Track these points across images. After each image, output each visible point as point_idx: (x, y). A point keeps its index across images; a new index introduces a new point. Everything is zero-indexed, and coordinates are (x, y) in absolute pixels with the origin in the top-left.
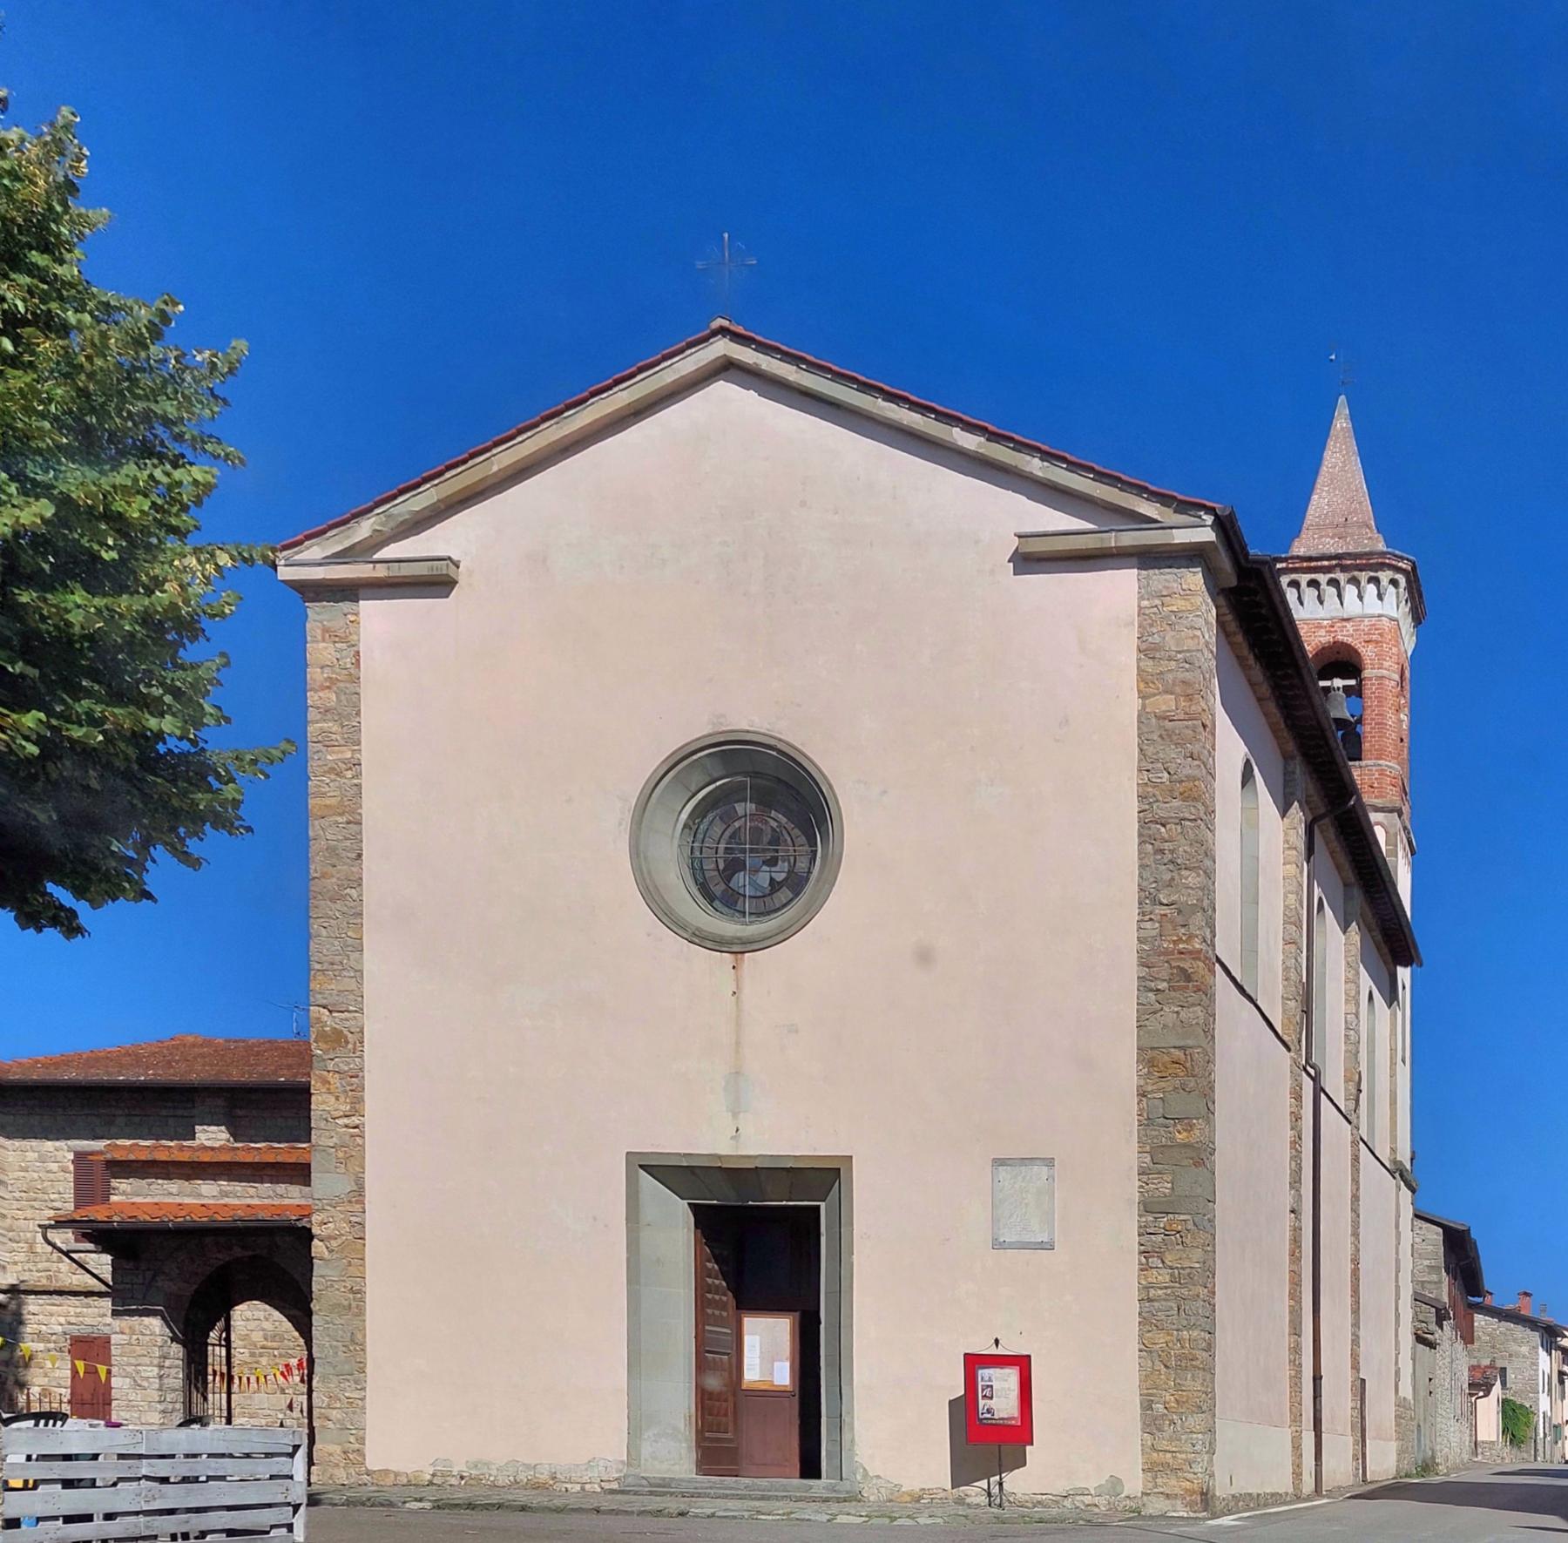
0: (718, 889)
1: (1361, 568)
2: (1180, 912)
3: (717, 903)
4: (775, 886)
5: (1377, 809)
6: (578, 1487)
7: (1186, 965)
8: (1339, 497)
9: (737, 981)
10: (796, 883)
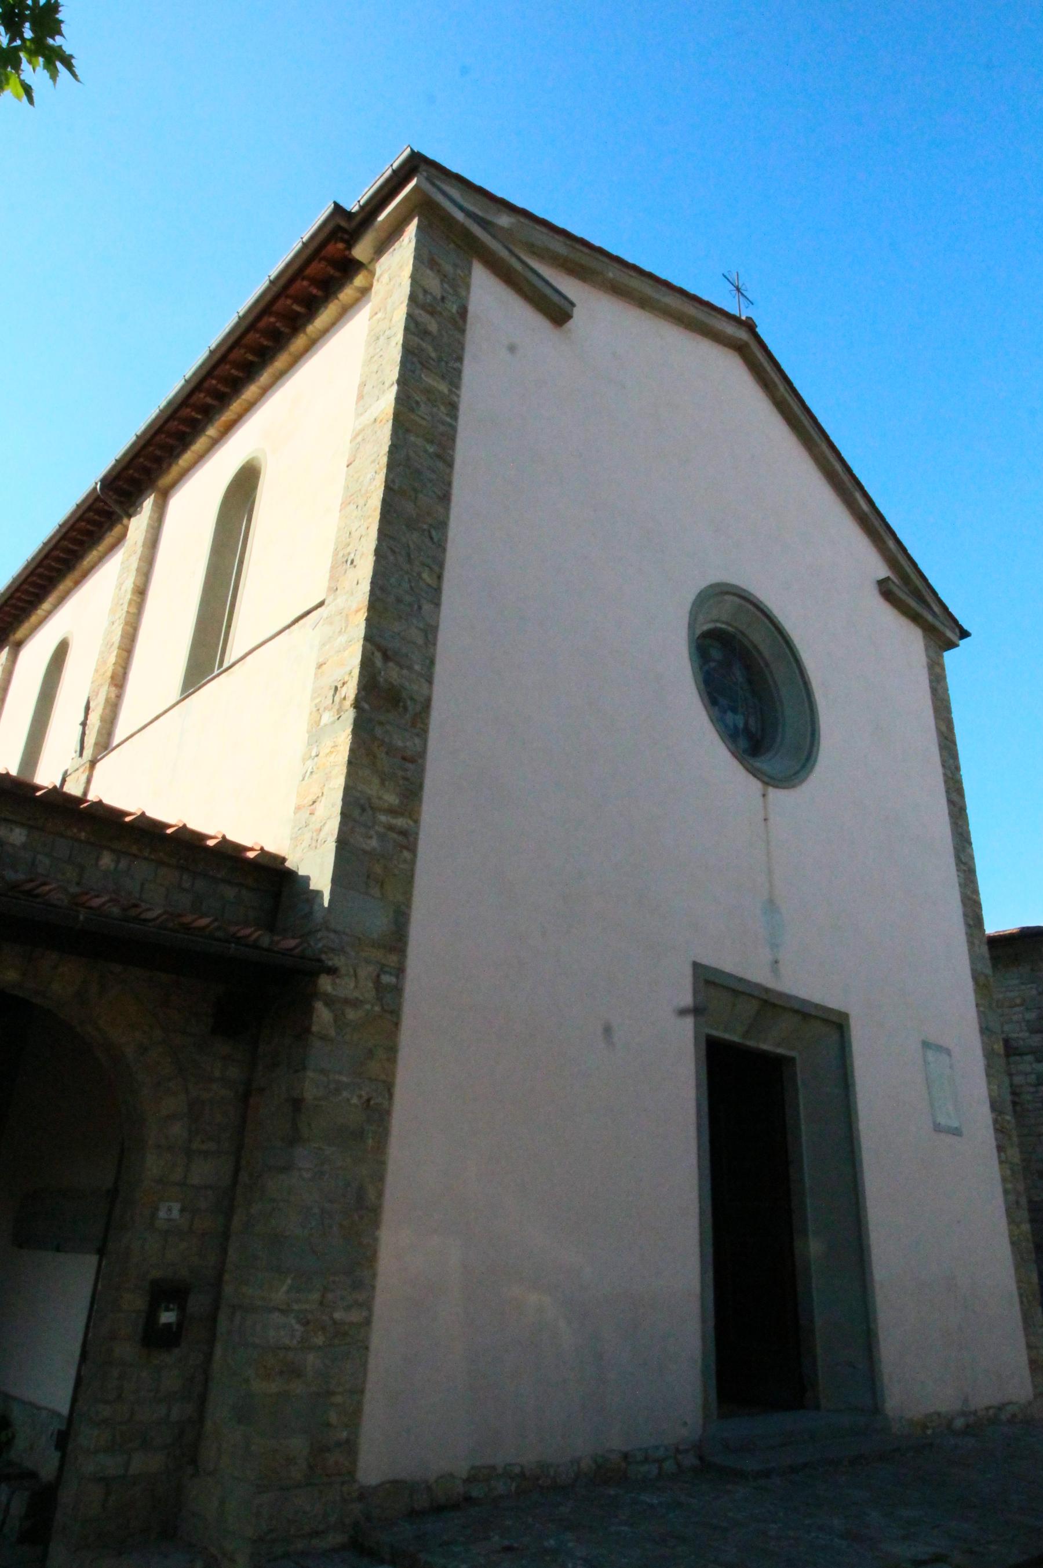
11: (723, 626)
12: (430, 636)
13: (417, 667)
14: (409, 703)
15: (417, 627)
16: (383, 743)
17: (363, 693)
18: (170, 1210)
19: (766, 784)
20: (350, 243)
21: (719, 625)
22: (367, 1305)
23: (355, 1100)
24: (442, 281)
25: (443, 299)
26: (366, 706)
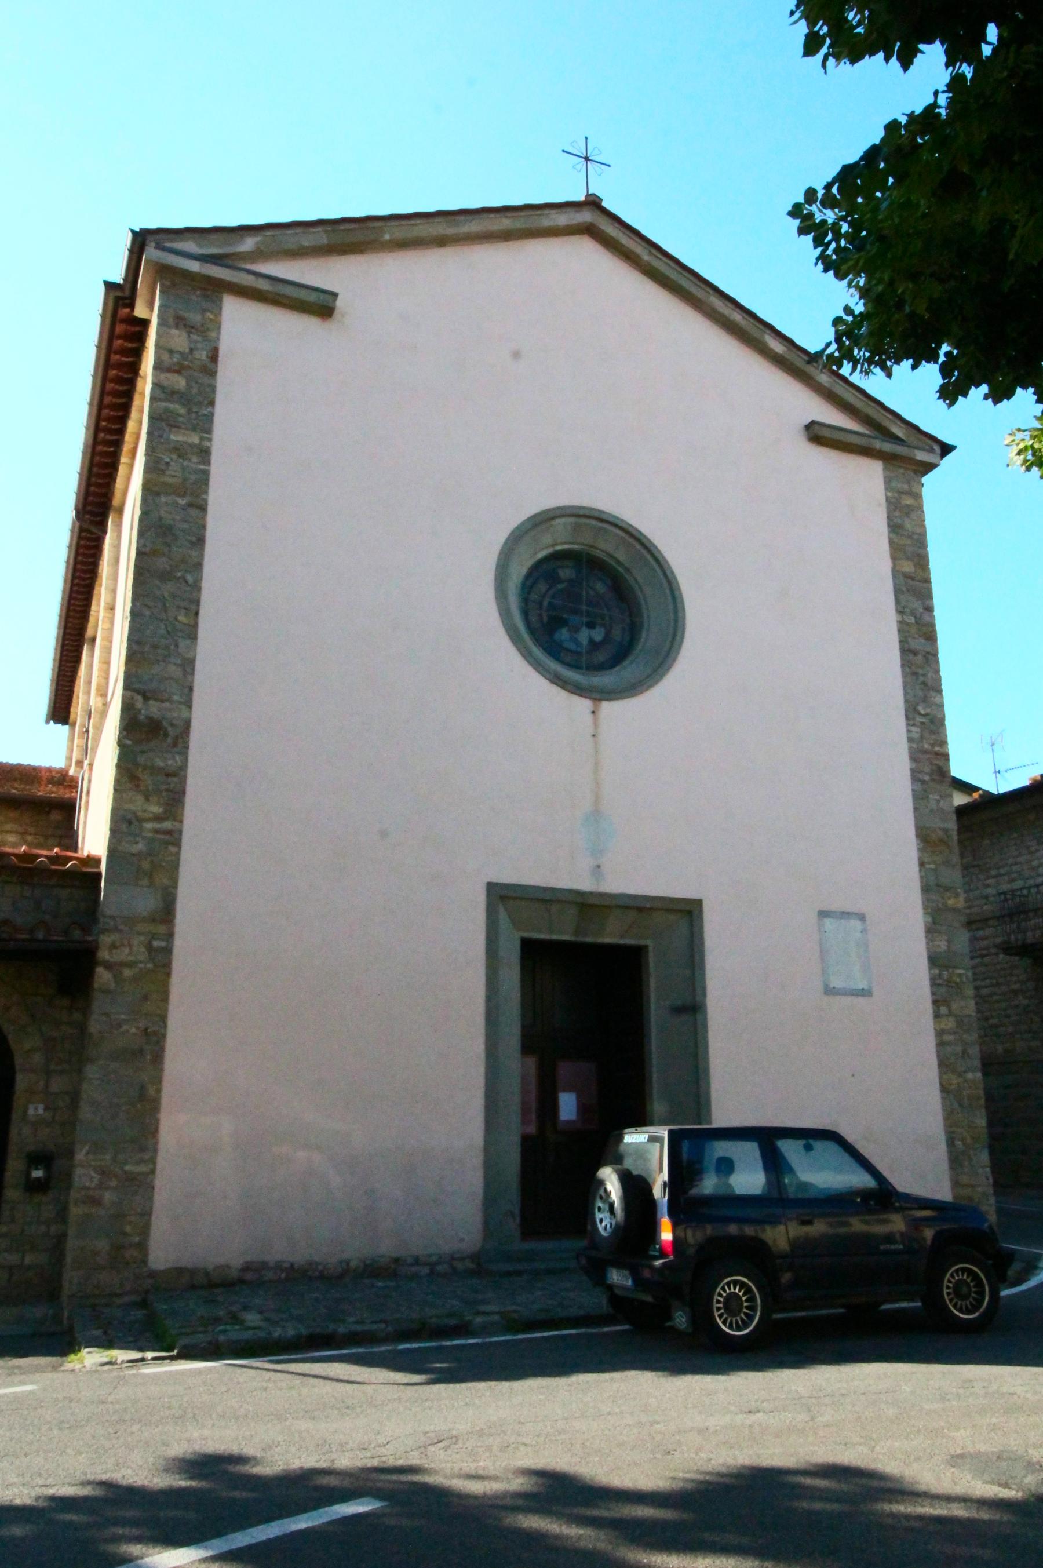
6: (426, 1270)
9: (596, 724)
11: (566, 547)
12: (188, 670)
13: (176, 698)
14: (170, 729)
15: (175, 664)
16: (145, 768)
17: (125, 733)
18: (36, 1109)
19: (594, 699)
20: (132, 306)
21: (559, 548)
22: (153, 1161)
23: (133, 1030)
24: (189, 333)
25: (191, 350)
26: (129, 742)
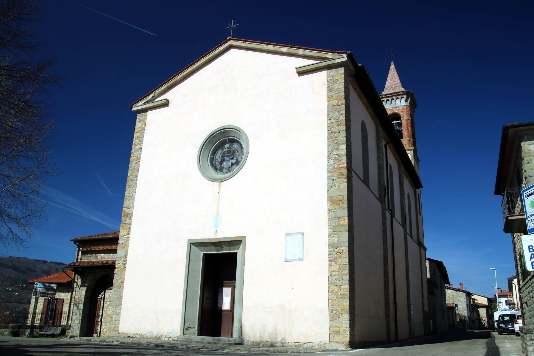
0: (218, 167)
1: (399, 95)
2: (339, 156)
3: (218, 171)
4: (233, 164)
5: (408, 150)
7: (342, 171)
8: (393, 82)
9: (220, 189)
10: (237, 163)
